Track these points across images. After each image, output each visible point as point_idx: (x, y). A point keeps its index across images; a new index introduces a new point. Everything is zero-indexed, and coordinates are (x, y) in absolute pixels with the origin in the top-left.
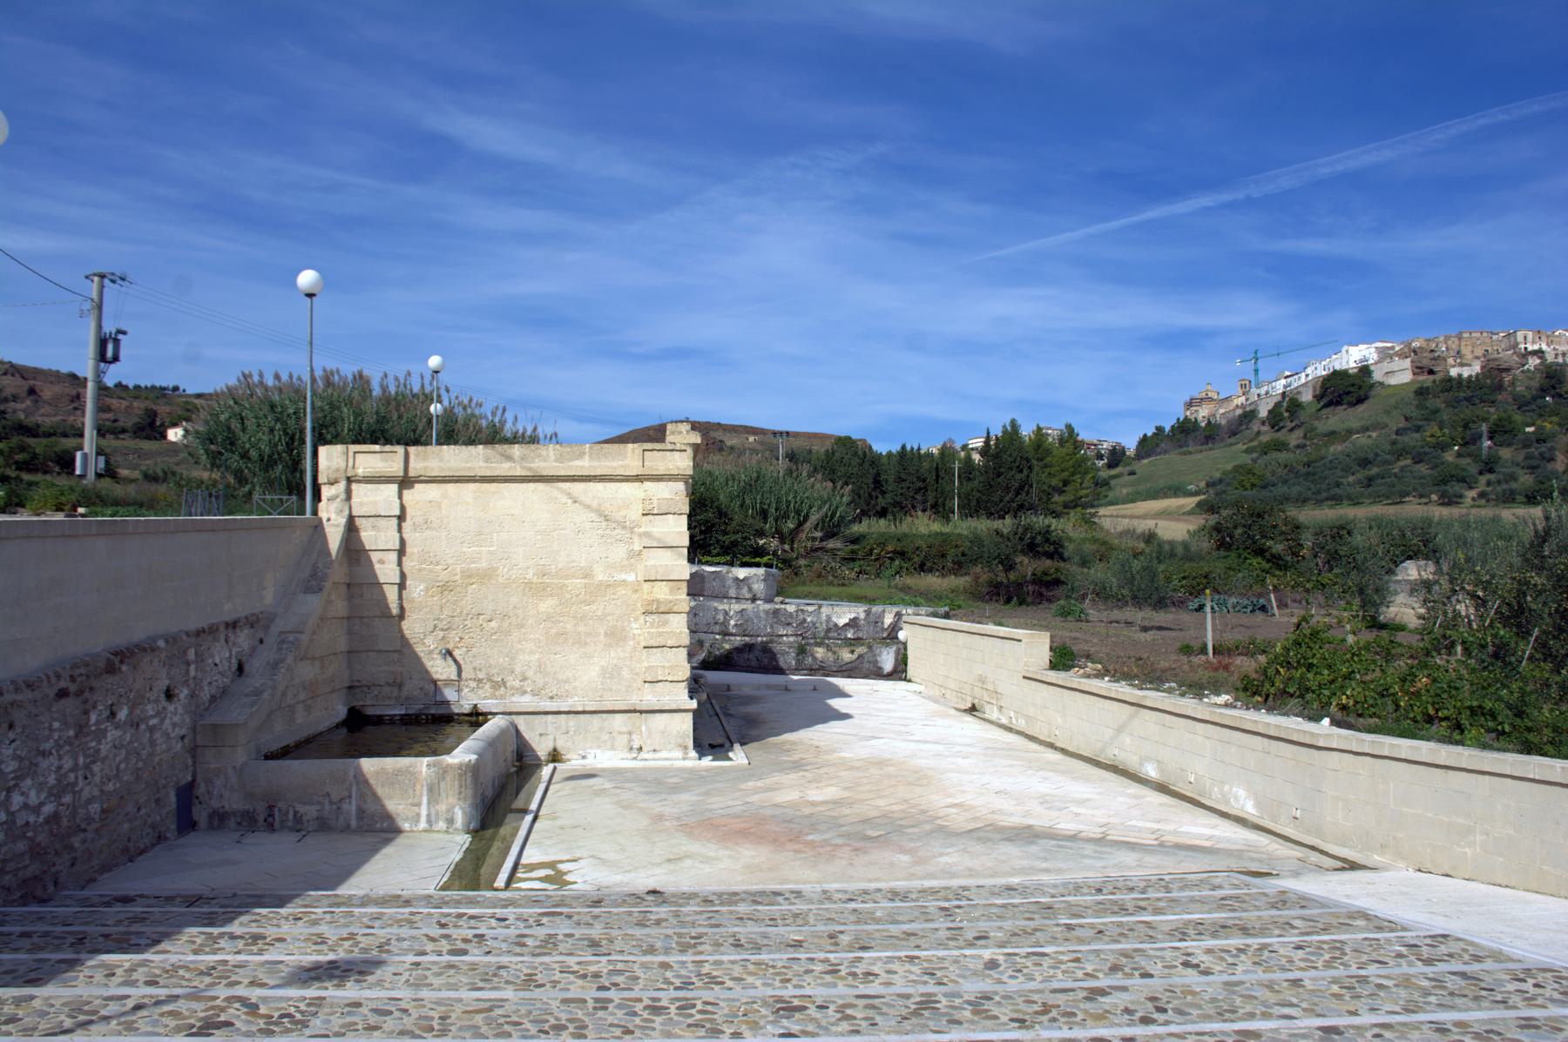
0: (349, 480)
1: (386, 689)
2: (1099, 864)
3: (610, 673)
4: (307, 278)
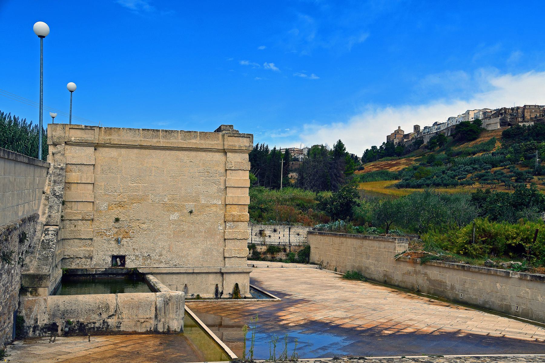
1: (84, 260)
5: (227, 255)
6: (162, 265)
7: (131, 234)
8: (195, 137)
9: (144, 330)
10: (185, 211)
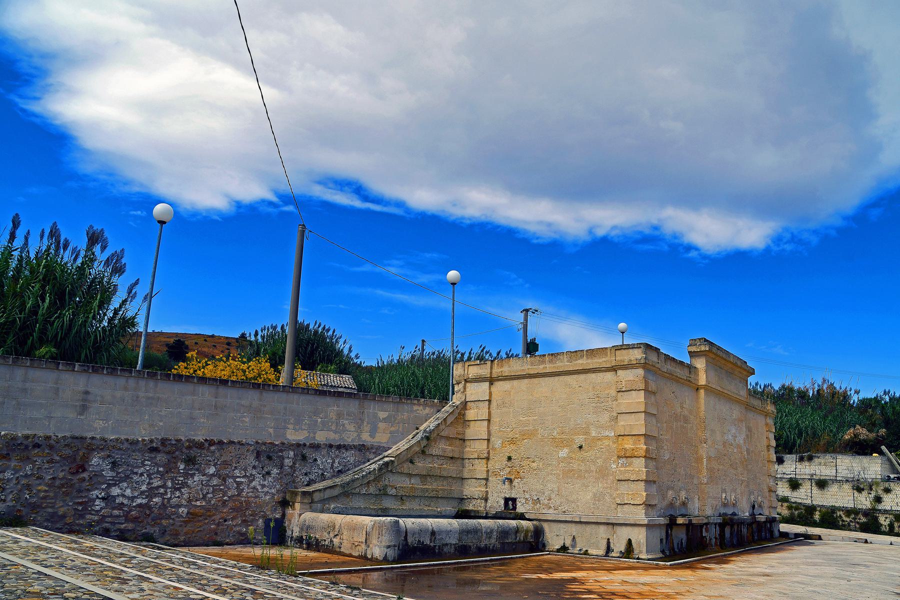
0: (466, 381)
2: (386, 459)
3: (598, 497)
4: (453, 274)
5: (484, 482)
6: (551, 511)
7: (522, 474)
8: (582, 357)
9: (356, 554)
10: (575, 446)
